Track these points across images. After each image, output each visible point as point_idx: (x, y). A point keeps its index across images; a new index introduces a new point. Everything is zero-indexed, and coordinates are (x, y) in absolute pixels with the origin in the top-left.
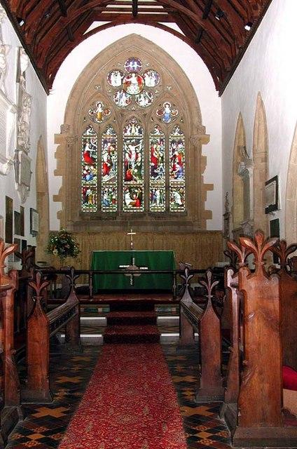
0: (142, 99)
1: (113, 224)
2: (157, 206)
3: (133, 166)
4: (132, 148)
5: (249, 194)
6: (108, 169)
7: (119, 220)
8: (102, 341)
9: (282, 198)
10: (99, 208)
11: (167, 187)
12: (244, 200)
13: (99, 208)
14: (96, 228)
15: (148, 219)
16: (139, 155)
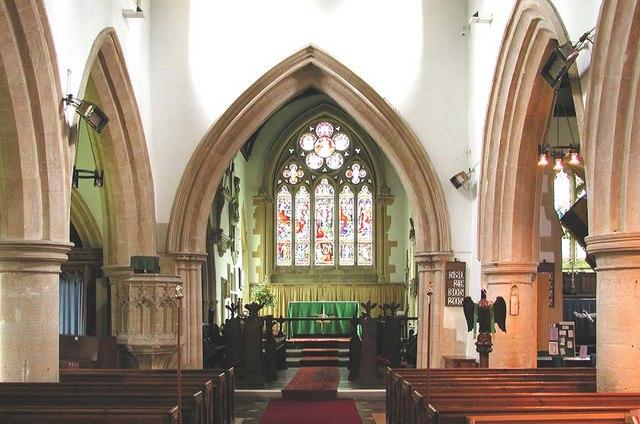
0: (333, 161)
1: (306, 277)
2: (346, 261)
3: (325, 223)
4: (324, 208)
5: (12, 21)
6: (301, 226)
7: (311, 273)
8: (281, 396)
9: (620, 51)
10: (294, 262)
11: (356, 243)
12: (48, 196)
13: (294, 262)
14: (292, 281)
15: (338, 272)
16: (330, 214)
